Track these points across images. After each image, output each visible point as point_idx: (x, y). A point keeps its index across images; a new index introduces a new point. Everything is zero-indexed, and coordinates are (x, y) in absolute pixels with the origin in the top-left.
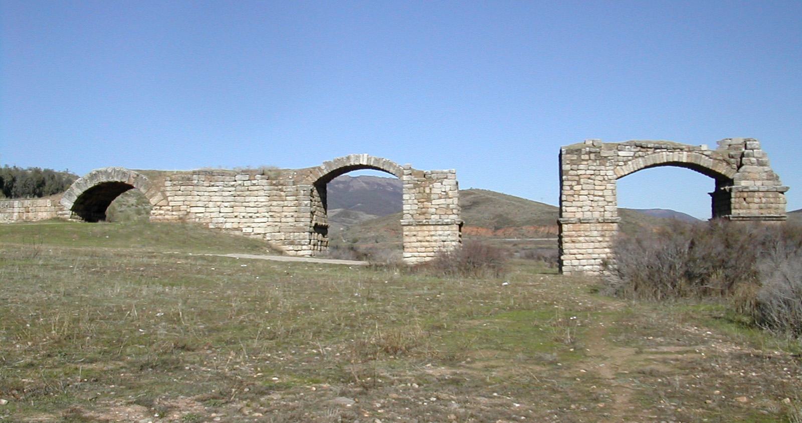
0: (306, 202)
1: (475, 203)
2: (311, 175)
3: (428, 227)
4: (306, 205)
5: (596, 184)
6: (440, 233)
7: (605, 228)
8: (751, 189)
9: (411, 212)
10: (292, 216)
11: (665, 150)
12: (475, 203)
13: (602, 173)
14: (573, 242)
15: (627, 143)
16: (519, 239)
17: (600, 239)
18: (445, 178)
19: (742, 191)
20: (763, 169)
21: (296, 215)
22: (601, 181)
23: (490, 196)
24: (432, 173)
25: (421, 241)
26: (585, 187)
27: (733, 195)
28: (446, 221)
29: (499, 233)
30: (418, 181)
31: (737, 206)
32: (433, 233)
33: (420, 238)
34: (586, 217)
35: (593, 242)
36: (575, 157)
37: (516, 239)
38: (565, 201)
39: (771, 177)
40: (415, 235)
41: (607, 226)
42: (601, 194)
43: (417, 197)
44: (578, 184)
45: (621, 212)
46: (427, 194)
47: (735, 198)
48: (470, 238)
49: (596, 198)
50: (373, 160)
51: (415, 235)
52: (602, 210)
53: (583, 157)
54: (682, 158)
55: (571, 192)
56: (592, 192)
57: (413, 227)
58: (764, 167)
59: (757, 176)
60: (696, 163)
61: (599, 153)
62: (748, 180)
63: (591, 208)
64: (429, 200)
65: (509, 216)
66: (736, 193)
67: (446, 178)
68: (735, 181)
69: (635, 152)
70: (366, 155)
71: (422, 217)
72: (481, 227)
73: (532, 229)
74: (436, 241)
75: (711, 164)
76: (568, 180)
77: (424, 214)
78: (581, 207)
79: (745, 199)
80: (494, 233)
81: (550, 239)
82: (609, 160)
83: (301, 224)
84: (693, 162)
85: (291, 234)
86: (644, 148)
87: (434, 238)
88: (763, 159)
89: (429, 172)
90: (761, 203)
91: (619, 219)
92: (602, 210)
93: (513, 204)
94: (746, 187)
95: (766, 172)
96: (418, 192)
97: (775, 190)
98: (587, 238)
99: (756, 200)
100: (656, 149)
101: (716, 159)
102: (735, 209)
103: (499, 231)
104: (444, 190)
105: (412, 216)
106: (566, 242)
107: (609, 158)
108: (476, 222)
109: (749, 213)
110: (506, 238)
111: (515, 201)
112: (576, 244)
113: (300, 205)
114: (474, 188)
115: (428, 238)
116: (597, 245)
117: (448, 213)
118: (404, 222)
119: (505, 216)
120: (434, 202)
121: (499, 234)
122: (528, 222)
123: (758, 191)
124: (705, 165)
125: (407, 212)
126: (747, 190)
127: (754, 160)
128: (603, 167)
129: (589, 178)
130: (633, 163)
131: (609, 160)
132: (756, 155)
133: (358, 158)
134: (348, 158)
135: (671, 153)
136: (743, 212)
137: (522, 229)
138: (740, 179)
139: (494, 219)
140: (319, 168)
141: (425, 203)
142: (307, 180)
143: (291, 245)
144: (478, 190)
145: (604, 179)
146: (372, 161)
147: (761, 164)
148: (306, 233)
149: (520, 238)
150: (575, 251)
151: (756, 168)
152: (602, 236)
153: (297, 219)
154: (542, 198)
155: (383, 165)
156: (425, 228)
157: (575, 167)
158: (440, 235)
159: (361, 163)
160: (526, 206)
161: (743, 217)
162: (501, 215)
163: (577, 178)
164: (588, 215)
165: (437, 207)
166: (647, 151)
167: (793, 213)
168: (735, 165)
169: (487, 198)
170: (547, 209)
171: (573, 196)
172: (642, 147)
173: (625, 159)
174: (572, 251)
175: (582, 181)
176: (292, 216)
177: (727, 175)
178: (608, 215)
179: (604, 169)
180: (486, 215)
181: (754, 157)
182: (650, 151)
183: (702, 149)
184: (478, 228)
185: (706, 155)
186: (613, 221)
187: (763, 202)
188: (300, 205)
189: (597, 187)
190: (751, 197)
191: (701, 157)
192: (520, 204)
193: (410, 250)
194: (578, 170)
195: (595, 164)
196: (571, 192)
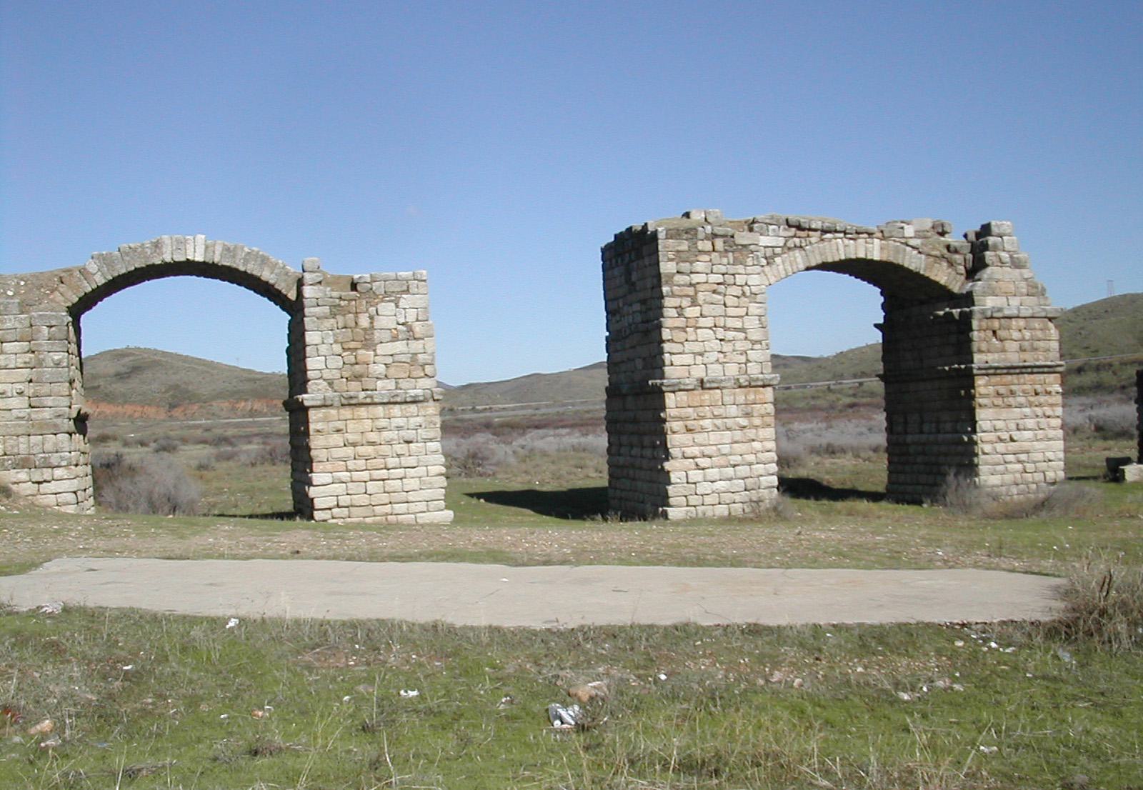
0: (57, 357)
1: (136, 370)
2: (62, 288)
3: (371, 408)
4: (57, 364)
5: (728, 304)
6: (401, 422)
7: (751, 397)
8: (1007, 312)
9: (327, 374)
10: (21, 394)
11: (842, 235)
12: (136, 370)
13: (740, 280)
14: (689, 430)
15: (772, 218)
16: (209, 421)
17: (744, 422)
18: (403, 292)
19: (992, 317)
20: (1021, 274)
21: (30, 389)
22: (738, 297)
23: (157, 358)
24: (373, 280)
25: (354, 445)
26: (707, 309)
27: (975, 324)
28: (412, 392)
29: (177, 413)
30: (340, 298)
31: (984, 346)
32: (383, 423)
33: (351, 437)
34: (712, 375)
35: (728, 429)
36: (684, 246)
37: (204, 421)
38: (668, 341)
39: (1035, 291)
40: (338, 431)
41: (755, 393)
42: (738, 324)
43: (340, 339)
44: (694, 303)
45: (778, 362)
46: (365, 329)
47: (979, 330)
48: (132, 422)
49: (730, 335)
50: (219, 249)
51: (338, 431)
52: (743, 359)
53: (701, 245)
54: (872, 252)
55: (680, 322)
56: (721, 322)
57: (333, 412)
58: (1024, 271)
59: (1012, 288)
60: (895, 261)
61: (732, 237)
62: (997, 296)
63: (722, 355)
64: (369, 344)
65: (190, 388)
66: (980, 320)
67: (407, 291)
68: (975, 298)
69: (787, 238)
70: (201, 238)
71: (355, 385)
72: (149, 405)
73: (226, 405)
74: (389, 443)
75: (923, 266)
76: (673, 295)
77: (358, 377)
78: (701, 354)
79: (994, 332)
80: (169, 414)
81: (256, 419)
82: (752, 252)
83: (46, 414)
84: (891, 259)
85: (21, 439)
86: (803, 229)
87: (386, 435)
88: (1020, 256)
89: (367, 277)
90: (1023, 339)
91: (776, 378)
92: (743, 359)
93: (194, 369)
94: (1000, 310)
95: (1026, 280)
96: (340, 325)
97: (1043, 314)
98: (718, 422)
99: (1016, 335)
100: (824, 231)
101: (929, 255)
102: (980, 351)
103: (176, 409)
104: (402, 321)
105: (331, 384)
106: (674, 433)
107: (752, 247)
108: (140, 397)
109: (1004, 360)
110: (188, 420)
111: (196, 364)
112: (696, 436)
113: (40, 363)
114: (132, 346)
115: (373, 437)
116: (738, 435)
117: (414, 374)
118: (313, 399)
119: (183, 386)
120: (381, 349)
121: (177, 414)
122: (219, 395)
123: (1018, 317)
124: (912, 267)
125: (317, 374)
126: (999, 315)
127: (1005, 256)
128: (740, 269)
129: (714, 292)
130: (783, 262)
131: (752, 252)
132: (1007, 247)
133: (181, 244)
134: (157, 245)
135: (852, 241)
136: (993, 359)
137: (211, 405)
138: (985, 294)
139: (166, 391)
140: (83, 271)
141: (360, 352)
142: (52, 300)
143: (23, 467)
144: (139, 348)
145: (744, 294)
146: (218, 253)
147: (1017, 264)
148: (60, 436)
149: (209, 419)
150: (695, 451)
151: (1009, 273)
152: (748, 415)
153: (34, 401)
154: (238, 359)
155: (246, 261)
156: (362, 411)
157: (685, 267)
158: (399, 428)
159: (191, 258)
160: (215, 372)
161: (996, 368)
162: (178, 386)
163: (690, 291)
164: (715, 371)
165: (389, 360)
166: (808, 236)
167: (582, 371)
168: (962, 268)
169: (154, 361)
170: (246, 375)
171: (683, 329)
172: (799, 228)
173: (769, 252)
174: (689, 452)
175: (701, 296)
176: (21, 394)
177: (950, 287)
178: (754, 370)
179: (742, 271)
180: (155, 386)
181: (1004, 251)
182: (815, 237)
183: (906, 235)
184: (143, 407)
185: (913, 248)
186: (767, 383)
187: (1027, 338)
188: (40, 363)
189: (731, 311)
190: (1004, 329)
191: (905, 250)
192: (205, 369)
193: (329, 466)
194: (691, 273)
195: (725, 261)
196: (680, 322)
